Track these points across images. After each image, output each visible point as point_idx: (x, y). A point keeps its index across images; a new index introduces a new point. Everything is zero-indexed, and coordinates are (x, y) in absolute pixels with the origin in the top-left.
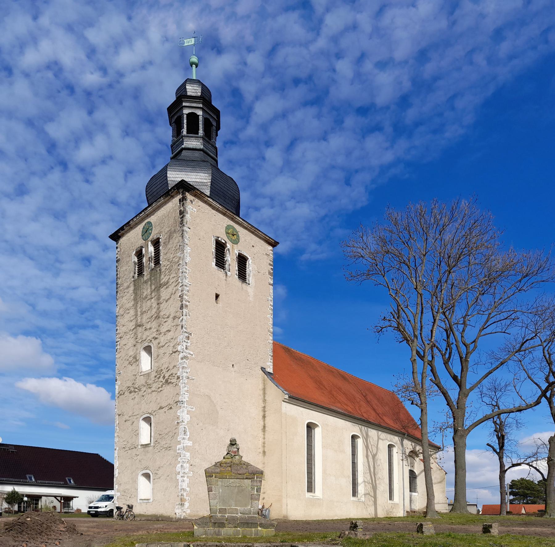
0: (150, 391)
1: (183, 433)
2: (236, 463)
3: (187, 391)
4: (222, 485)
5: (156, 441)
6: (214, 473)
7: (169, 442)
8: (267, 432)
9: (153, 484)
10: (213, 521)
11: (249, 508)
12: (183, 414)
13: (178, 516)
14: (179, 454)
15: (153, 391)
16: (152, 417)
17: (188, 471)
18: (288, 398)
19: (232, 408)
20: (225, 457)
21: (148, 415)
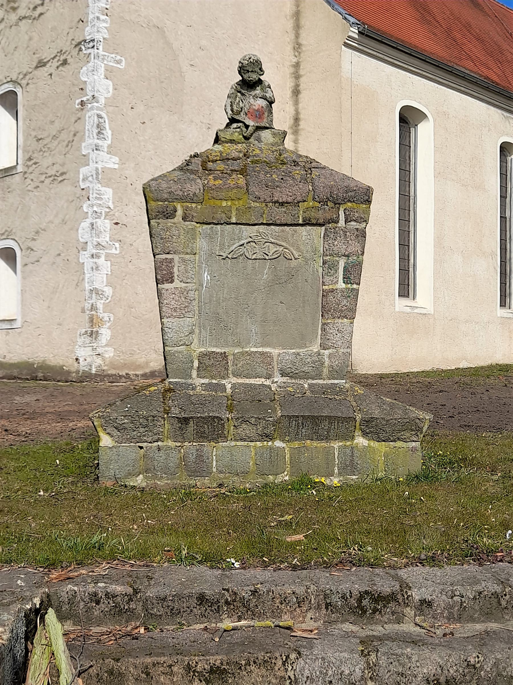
0: (13, 17)
1: (96, 131)
2: (263, 157)
3: (106, 12)
4: (211, 254)
5: (30, 159)
6: (181, 200)
7: (59, 159)
8: (302, 133)
9: (24, 278)
10: (175, 411)
11: (315, 348)
12: (96, 77)
13: (83, 366)
14: (84, 192)
15: (21, 19)
16: (19, 91)
17: (107, 239)
18: (356, 36)
19: (219, 65)
20: (221, 135)
21: (9, 87)
